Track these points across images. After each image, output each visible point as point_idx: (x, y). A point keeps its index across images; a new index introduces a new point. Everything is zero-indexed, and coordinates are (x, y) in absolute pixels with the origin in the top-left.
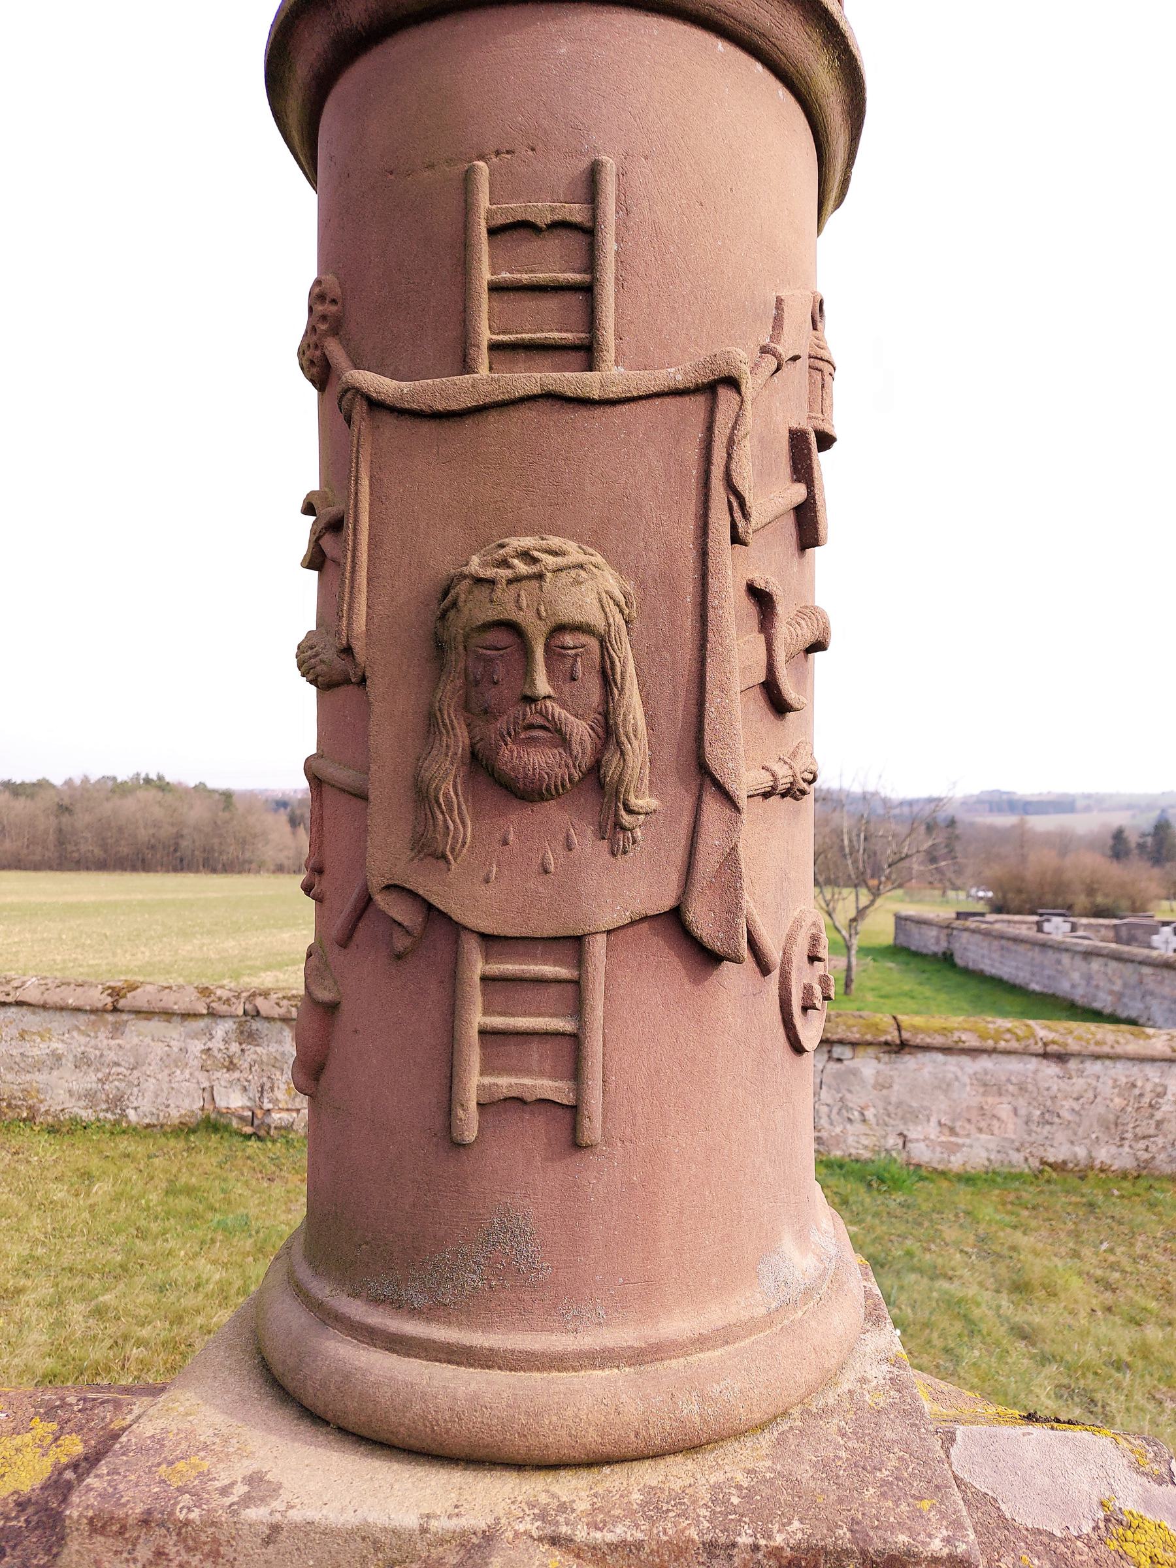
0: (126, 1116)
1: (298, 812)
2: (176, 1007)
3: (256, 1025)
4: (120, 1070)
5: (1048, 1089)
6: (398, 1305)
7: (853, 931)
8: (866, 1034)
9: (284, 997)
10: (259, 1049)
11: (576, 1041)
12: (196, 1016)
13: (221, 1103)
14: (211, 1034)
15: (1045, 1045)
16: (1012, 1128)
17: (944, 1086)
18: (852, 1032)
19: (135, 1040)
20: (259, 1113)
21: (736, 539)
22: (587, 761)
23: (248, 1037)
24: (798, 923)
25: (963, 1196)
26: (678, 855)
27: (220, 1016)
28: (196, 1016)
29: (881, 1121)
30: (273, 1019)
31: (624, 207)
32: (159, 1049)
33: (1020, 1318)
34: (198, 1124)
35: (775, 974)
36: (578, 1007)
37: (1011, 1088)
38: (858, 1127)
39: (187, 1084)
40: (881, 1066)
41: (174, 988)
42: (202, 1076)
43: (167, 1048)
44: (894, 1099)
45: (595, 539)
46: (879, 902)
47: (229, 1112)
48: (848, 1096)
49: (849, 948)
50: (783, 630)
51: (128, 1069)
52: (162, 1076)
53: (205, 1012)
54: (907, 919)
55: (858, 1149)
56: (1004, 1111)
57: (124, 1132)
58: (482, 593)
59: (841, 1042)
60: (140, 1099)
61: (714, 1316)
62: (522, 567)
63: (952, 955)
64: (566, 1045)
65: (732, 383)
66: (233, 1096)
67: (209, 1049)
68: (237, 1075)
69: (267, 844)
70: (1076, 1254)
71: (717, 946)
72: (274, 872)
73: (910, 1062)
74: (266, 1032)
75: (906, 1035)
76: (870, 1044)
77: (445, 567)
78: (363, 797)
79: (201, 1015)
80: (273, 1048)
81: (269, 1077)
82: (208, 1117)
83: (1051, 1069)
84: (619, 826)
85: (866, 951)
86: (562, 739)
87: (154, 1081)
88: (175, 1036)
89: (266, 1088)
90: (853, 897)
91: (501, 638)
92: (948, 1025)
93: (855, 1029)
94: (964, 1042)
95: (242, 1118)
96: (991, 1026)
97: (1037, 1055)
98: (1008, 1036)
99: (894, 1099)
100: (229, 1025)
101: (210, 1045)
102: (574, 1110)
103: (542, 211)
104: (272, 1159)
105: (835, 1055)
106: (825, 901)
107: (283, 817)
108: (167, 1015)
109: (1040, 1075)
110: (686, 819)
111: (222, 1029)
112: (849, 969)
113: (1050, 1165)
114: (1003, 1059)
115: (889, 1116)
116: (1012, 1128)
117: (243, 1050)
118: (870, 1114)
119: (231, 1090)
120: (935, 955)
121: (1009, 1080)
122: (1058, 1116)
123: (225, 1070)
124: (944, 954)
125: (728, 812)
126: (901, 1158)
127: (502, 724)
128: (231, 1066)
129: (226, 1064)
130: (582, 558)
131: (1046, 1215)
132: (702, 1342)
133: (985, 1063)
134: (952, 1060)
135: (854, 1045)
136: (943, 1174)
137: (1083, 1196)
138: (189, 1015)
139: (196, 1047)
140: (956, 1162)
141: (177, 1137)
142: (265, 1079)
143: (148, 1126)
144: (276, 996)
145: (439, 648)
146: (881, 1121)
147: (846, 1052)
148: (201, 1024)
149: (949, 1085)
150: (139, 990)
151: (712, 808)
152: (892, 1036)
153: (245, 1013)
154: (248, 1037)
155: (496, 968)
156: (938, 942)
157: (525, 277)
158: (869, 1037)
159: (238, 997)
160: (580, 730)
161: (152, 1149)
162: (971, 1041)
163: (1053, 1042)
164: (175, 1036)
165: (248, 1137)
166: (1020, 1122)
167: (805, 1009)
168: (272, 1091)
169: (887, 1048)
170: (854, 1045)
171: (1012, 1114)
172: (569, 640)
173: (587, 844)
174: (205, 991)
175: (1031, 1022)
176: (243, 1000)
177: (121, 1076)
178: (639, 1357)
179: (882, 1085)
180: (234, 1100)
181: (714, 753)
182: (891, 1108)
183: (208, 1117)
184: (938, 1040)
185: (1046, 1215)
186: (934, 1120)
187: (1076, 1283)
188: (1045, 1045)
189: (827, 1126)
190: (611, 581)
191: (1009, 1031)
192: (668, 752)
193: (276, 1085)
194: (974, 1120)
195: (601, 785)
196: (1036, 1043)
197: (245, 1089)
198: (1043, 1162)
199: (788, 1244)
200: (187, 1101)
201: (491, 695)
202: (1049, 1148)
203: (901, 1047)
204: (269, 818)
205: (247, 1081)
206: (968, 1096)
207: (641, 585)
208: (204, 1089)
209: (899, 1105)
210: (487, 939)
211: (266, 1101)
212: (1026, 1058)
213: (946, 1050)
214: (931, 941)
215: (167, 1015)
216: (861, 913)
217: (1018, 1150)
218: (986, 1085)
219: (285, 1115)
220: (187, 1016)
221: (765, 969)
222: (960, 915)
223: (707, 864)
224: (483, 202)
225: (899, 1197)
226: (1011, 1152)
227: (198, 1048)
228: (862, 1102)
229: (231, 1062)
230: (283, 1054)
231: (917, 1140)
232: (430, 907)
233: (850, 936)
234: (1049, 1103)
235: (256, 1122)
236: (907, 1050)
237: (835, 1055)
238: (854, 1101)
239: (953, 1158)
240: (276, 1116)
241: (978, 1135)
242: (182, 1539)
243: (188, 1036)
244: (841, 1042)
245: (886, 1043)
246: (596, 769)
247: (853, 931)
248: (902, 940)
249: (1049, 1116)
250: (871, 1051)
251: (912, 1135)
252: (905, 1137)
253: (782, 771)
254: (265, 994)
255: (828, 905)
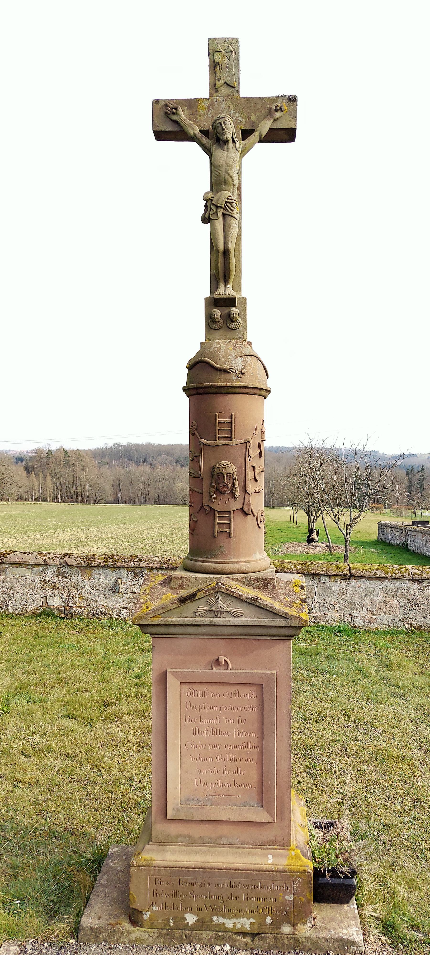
0: (8, 610)
1: (30, 464)
2: (30, 561)
3: (65, 569)
4: (4, 589)
5: (414, 595)
6: (207, 558)
7: (348, 531)
8: (335, 571)
9: (78, 557)
10: (67, 580)
11: (230, 524)
12: (39, 565)
13: (51, 604)
14: (45, 573)
15: (413, 575)
16: (399, 611)
17: (369, 594)
18: (329, 570)
19: (11, 576)
20: (67, 608)
21: (249, 460)
22: (231, 489)
23: (62, 574)
24: (259, 510)
25: (373, 638)
26: (243, 501)
27: (49, 565)
28: (39, 565)
29: (342, 609)
30: (73, 566)
31: (235, 419)
32: (22, 580)
33: (385, 675)
34: (41, 613)
35: (256, 517)
36: (230, 520)
37: (398, 594)
38: (332, 612)
39: (35, 595)
40: (342, 585)
41: (27, 553)
42: (41, 592)
43: (26, 580)
44: (347, 600)
45: (231, 462)
46: (363, 515)
47: (54, 608)
48: (327, 598)
49: (346, 540)
50: (256, 470)
51: (8, 589)
52: (24, 592)
53: (43, 563)
54: (385, 525)
55: (332, 621)
56: (395, 605)
57: (7, 617)
58: (218, 469)
59: (324, 575)
60: (14, 602)
61: (247, 559)
62: (223, 466)
63: (407, 544)
64: (228, 524)
65: (249, 442)
66: (55, 600)
67: (45, 580)
68: (57, 591)
69: (12, 483)
70: (415, 656)
71: (247, 513)
72: (17, 500)
73: (354, 583)
74: (70, 572)
75: (352, 572)
76: (337, 575)
77: (213, 464)
78: (202, 494)
79: (41, 565)
80: (73, 579)
81: (72, 592)
82: (45, 610)
83: (415, 586)
84: (235, 497)
85: (354, 542)
86: (228, 487)
87: (20, 594)
88: (30, 574)
89: (70, 597)
90: (349, 513)
91: (221, 474)
92: (372, 567)
93: (330, 569)
94: (378, 574)
95: (60, 611)
96: (390, 568)
97: (409, 580)
98: (397, 572)
99: (347, 600)
100: (53, 569)
101: (45, 578)
102: (230, 533)
103: (225, 420)
104: (76, 626)
105: (322, 581)
106: (334, 515)
107: (21, 467)
108: (26, 565)
109: (411, 588)
110: (243, 496)
111: (50, 571)
112: (346, 550)
113: (414, 627)
114: (394, 582)
115: (345, 607)
116: (399, 611)
117: (59, 580)
118: (337, 606)
119: (54, 598)
120: (399, 544)
121: (397, 591)
122: (418, 606)
123: (52, 589)
124: (403, 544)
125: (249, 496)
126: (350, 625)
127: (220, 485)
128: (54, 588)
129: (52, 586)
130: (230, 465)
131: (407, 644)
132: (245, 562)
133: (387, 584)
134: (373, 582)
135: (330, 576)
136: (368, 631)
137: (425, 638)
138: (35, 565)
139: (39, 579)
140: (374, 626)
141: (32, 618)
142: (70, 593)
143: (18, 614)
144: (73, 556)
145: (212, 475)
146: (342, 609)
147: (327, 579)
148: (40, 569)
149: (371, 593)
150: (12, 554)
151: (247, 495)
152: (347, 572)
153: (61, 564)
154: (62, 574)
155: (219, 515)
156: (400, 539)
157: (223, 428)
158: (336, 573)
159: (57, 557)
160: (230, 485)
161: (23, 623)
162: (381, 574)
163: (416, 574)
164: (30, 574)
165: (62, 618)
166: (402, 609)
167: (261, 522)
168: (73, 598)
169: (344, 577)
170: (330, 576)
171: (398, 606)
172: (229, 475)
173: (231, 500)
174: (41, 555)
175: (409, 566)
176: (59, 558)
177: (5, 592)
178: (237, 562)
179: (343, 594)
180: (56, 602)
181: (247, 488)
182: (346, 604)
183: (45, 610)
184: (367, 574)
185: (407, 644)
186: (364, 608)
187: (411, 665)
188: (413, 575)
189: (318, 611)
190: (234, 467)
191: (397, 569)
192: (241, 488)
193: (75, 596)
194: (382, 608)
195: (233, 492)
196: (409, 575)
197: (61, 598)
198: (411, 626)
199: (258, 553)
200: (35, 603)
201: (219, 481)
202: (414, 620)
203: (351, 577)
204: (13, 468)
205: (62, 594)
206: (379, 598)
207: (238, 467)
208: (42, 598)
209: (350, 602)
210: (219, 512)
211: (70, 602)
212: (405, 581)
213: (370, 578)
214: (396, 538)
215: (26, 565)
216: (353, 521)
217: (401, 621)
218: (386, 592)
219: (79, 609)
220: (34, 565)
221: (254, 516)
222: (414, 523)
223: (246, 502)
224: (218, 419)
225: (346, 638)
226: (397, 622)
227: (39, 580)
228: (333, 601)
229: (55, 586)
230: (78, 582)
231: (357, 617)
232: (211, 508)
233: (347, 533)
234: (414, 600)
235: (66, 612)
236: (353, 578)
237: (322, 581)
238: (330, 600)
239: (372, 625)
240: (75, 609)
241: (384, 615)
242: (185, 579)
243: (35, 574)
244: (324, 575)
245: (344, 575)
246: (232, 490)
247: (348, 531)
248: (382, 537)
249: (415, 606)
250: (337, 578)
251: (355, 615)
252: (352, 615)
253: (257, 489)
254: (69, 556)
255: (335, 518)
